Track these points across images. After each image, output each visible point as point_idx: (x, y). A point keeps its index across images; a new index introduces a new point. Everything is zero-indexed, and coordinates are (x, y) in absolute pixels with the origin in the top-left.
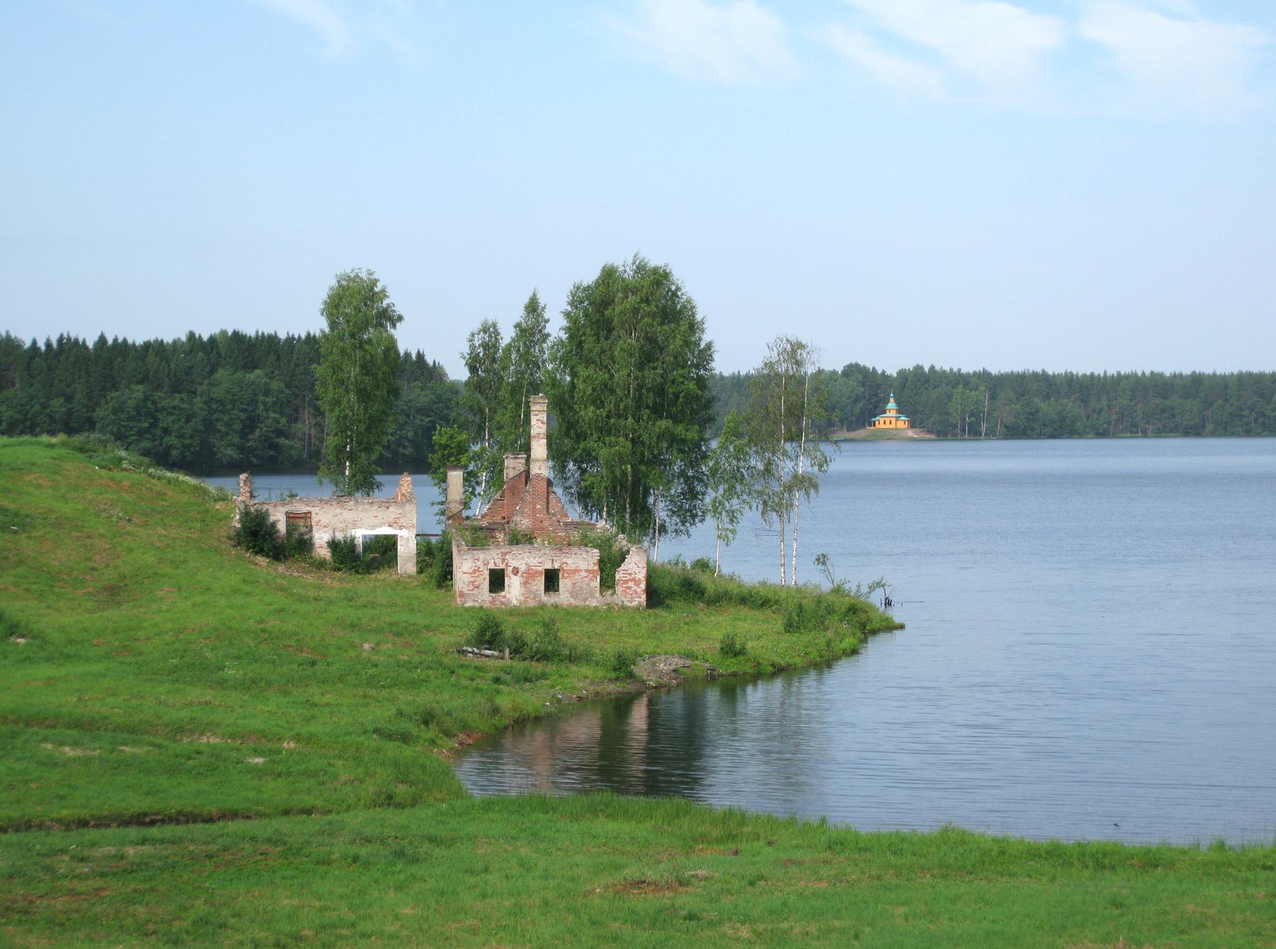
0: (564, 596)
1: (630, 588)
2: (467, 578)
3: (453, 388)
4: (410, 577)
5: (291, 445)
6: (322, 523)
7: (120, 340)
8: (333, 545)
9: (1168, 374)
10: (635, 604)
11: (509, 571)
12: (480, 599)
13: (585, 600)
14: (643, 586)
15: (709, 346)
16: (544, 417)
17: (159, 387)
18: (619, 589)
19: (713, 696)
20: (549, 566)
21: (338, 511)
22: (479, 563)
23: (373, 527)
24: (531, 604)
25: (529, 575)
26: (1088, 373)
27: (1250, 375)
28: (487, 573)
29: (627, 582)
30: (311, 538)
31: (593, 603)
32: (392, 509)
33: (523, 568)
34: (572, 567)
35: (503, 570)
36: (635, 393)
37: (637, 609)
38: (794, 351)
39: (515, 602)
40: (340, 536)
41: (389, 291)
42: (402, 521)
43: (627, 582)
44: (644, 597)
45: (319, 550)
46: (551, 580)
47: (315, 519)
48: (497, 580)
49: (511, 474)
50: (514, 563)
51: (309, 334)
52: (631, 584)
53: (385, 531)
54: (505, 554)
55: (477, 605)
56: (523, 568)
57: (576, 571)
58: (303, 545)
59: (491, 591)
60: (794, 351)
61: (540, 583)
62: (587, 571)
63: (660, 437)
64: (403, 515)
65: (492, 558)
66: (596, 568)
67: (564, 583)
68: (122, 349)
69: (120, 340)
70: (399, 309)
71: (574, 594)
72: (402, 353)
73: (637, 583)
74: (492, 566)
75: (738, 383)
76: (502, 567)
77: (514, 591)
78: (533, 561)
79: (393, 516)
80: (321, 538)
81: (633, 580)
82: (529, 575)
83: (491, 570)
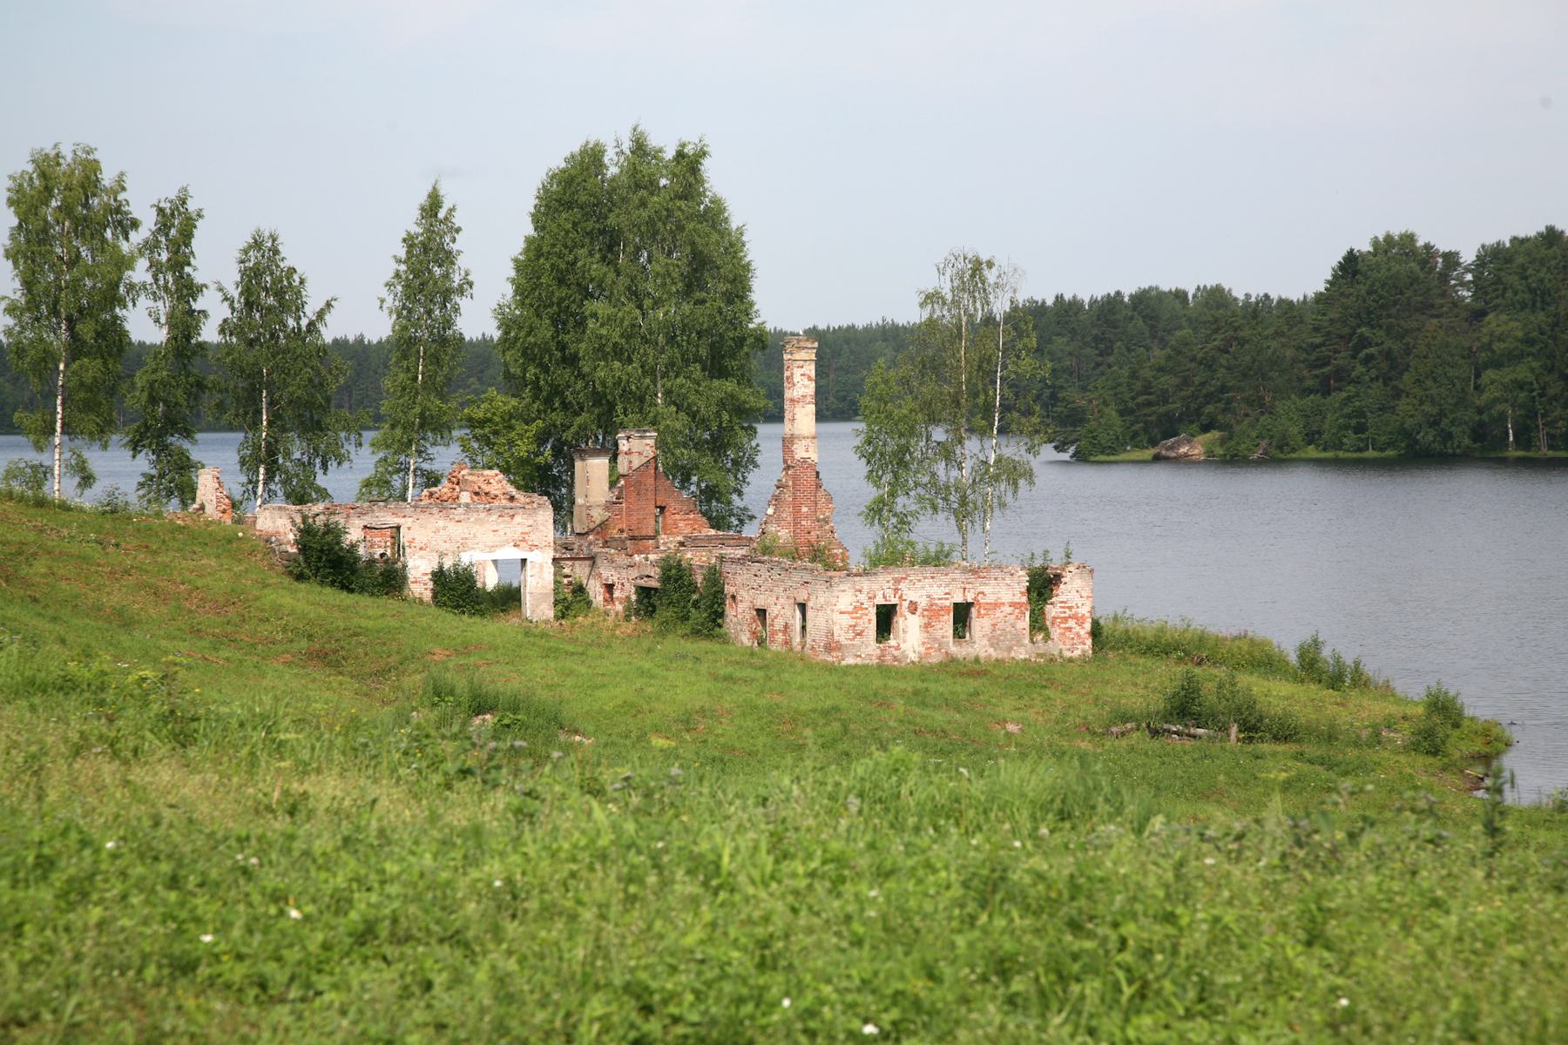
0: (980, 644)
1: (1070, 629)
2: (846, 620)
4: (547, 622)
6: (417, 544)
8: (439, 576)
9: (1301, 277)
10: (1077, 653)
12: (864, 652)
13: (1010, 649)
14: (1088, 626)
16: (811, 369)
18: (1055, 632)
19: (86, 883)
20: (959, 599)
21: (441, 523)
22: (863, 597)
24: (936, 658)
28: (874, 611)
29: (1066, 619)
30: (405, 567)
31: (1021, 654)
32: (518, 519)
33: (923, 603)
34: (990, 599)
35: (894, 606)
37: (1083, 658)
38: (516, 260)
39: (913, 657)
40: (448, 564)
42: (534, 538)
43: (1066, 619)
44: (1089, 642)
45: (412, 586)
46: (962, 614)
47: (405, 537)
48: (886, 618)
50: (911, 595)
52: (1072, 623)
54: (897, 581)
55: (859, 661)
56: (923, 603)
57: (997, 605)
58: (390, 579)
59: (878, 641)
60: (516, 260)
61: (947, 624)
62: (1012, 605)
63: (722, 404)
65: (881, 588)
66: (1024, 599)
67: (980, 625)
68: (535, 250)
71: (994, 641)
73: (1080, 621)
76: (894, 601)
78: (937, 591)
79: (520, 529)
80: (419, 569)
81: (1074, 617)
82: (933, 612)
83: (878, 607)
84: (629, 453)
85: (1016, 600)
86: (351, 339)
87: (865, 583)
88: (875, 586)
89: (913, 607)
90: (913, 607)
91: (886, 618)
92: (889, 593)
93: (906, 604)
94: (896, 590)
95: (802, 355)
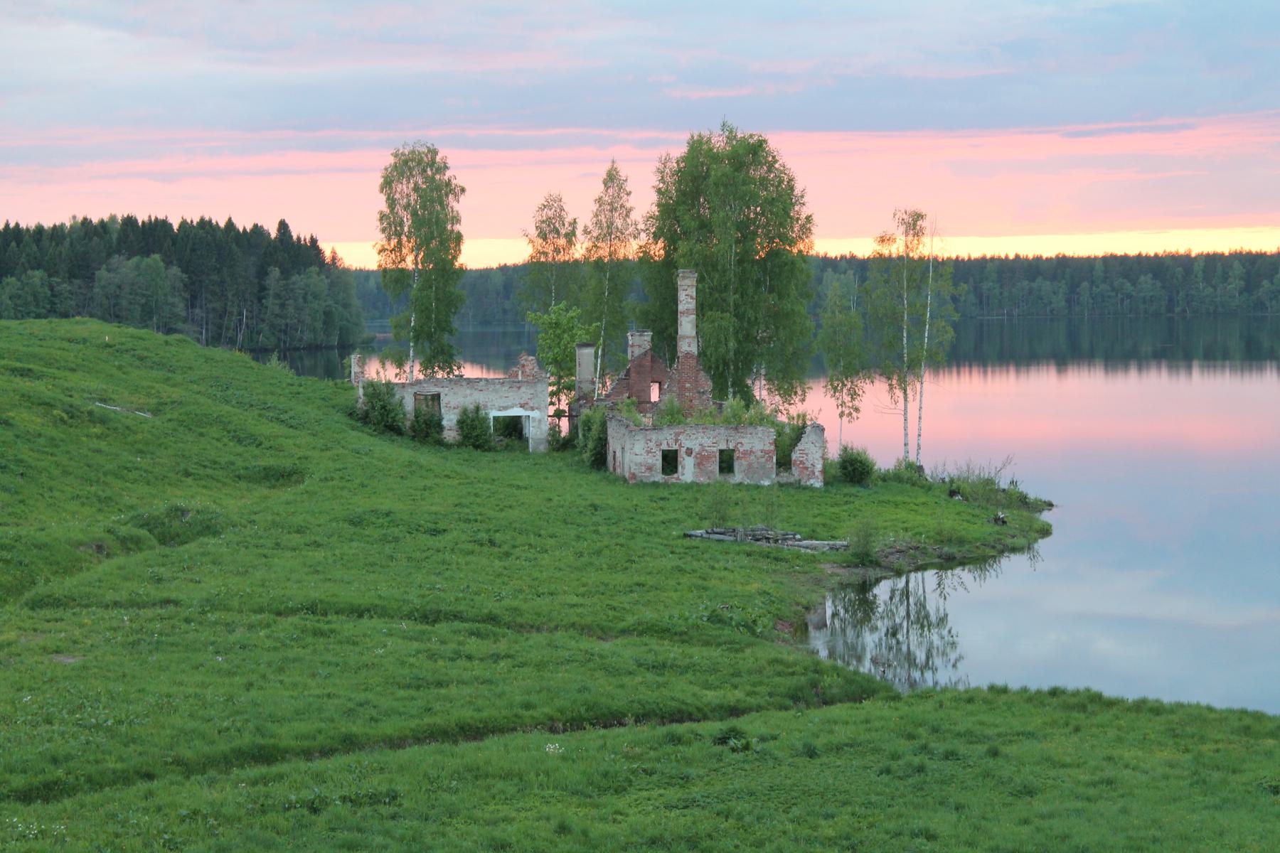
3: (453, 264)
5: (1246, 294)
7: (12, 225)
8: (461, 423)
9: (1031, 256)
11: (682, 453)
15: (809, 218)
16: (693, 292)
17: (56, 273)
20: (723, 447)
21: (468, 391)
22: (651, 445)
23: (505, 408)
25: (701, 461)
26: (954, 257)
27: (1113, 258)
32: (523, 389)
33: (697, 449)
34: (747, 447)
35: (676, 451)
36: (728, 272)
41: (450, 163)
46: (727, 462)
48: (670, 461)
49: (637, 352)
50: (687, 444)
51: (202, 219)
53: (516, 412)
54: (677, 434)
56: (697, 449)
64: (534, 396)
65: (666, 440)
66: (772, 447)
69: (12, 225)
70: (459, 181)
72: (295, 237)
74: (665, 447)
75: (462, 271)
76: (675, 447)
77: (687, 471)
78: (707, 442)
80: (450, 419)
84: (632, 346)
85: (767, 448)
86: (1011, 257)
87: (654, 436)
88: (661, 437)
89: (689, 452)
90: (689, 452)
91: (670, 461)
92: (671, 442)
93: (684, 450)
94: (676, 441)
95: (688, 282)
